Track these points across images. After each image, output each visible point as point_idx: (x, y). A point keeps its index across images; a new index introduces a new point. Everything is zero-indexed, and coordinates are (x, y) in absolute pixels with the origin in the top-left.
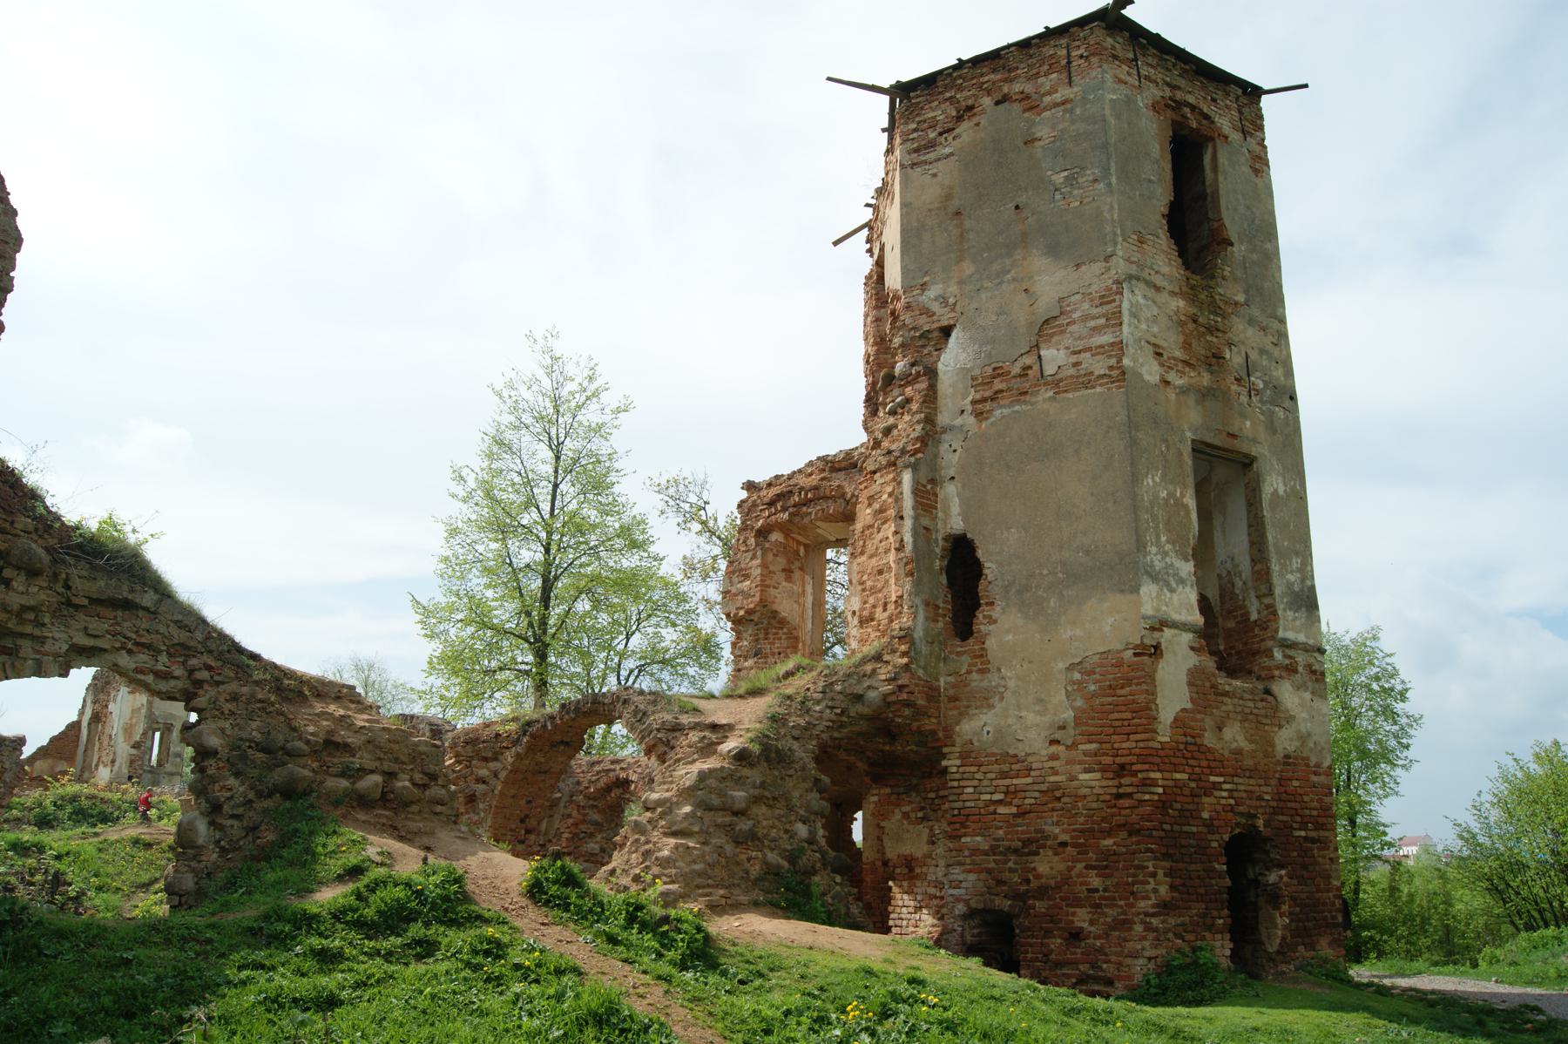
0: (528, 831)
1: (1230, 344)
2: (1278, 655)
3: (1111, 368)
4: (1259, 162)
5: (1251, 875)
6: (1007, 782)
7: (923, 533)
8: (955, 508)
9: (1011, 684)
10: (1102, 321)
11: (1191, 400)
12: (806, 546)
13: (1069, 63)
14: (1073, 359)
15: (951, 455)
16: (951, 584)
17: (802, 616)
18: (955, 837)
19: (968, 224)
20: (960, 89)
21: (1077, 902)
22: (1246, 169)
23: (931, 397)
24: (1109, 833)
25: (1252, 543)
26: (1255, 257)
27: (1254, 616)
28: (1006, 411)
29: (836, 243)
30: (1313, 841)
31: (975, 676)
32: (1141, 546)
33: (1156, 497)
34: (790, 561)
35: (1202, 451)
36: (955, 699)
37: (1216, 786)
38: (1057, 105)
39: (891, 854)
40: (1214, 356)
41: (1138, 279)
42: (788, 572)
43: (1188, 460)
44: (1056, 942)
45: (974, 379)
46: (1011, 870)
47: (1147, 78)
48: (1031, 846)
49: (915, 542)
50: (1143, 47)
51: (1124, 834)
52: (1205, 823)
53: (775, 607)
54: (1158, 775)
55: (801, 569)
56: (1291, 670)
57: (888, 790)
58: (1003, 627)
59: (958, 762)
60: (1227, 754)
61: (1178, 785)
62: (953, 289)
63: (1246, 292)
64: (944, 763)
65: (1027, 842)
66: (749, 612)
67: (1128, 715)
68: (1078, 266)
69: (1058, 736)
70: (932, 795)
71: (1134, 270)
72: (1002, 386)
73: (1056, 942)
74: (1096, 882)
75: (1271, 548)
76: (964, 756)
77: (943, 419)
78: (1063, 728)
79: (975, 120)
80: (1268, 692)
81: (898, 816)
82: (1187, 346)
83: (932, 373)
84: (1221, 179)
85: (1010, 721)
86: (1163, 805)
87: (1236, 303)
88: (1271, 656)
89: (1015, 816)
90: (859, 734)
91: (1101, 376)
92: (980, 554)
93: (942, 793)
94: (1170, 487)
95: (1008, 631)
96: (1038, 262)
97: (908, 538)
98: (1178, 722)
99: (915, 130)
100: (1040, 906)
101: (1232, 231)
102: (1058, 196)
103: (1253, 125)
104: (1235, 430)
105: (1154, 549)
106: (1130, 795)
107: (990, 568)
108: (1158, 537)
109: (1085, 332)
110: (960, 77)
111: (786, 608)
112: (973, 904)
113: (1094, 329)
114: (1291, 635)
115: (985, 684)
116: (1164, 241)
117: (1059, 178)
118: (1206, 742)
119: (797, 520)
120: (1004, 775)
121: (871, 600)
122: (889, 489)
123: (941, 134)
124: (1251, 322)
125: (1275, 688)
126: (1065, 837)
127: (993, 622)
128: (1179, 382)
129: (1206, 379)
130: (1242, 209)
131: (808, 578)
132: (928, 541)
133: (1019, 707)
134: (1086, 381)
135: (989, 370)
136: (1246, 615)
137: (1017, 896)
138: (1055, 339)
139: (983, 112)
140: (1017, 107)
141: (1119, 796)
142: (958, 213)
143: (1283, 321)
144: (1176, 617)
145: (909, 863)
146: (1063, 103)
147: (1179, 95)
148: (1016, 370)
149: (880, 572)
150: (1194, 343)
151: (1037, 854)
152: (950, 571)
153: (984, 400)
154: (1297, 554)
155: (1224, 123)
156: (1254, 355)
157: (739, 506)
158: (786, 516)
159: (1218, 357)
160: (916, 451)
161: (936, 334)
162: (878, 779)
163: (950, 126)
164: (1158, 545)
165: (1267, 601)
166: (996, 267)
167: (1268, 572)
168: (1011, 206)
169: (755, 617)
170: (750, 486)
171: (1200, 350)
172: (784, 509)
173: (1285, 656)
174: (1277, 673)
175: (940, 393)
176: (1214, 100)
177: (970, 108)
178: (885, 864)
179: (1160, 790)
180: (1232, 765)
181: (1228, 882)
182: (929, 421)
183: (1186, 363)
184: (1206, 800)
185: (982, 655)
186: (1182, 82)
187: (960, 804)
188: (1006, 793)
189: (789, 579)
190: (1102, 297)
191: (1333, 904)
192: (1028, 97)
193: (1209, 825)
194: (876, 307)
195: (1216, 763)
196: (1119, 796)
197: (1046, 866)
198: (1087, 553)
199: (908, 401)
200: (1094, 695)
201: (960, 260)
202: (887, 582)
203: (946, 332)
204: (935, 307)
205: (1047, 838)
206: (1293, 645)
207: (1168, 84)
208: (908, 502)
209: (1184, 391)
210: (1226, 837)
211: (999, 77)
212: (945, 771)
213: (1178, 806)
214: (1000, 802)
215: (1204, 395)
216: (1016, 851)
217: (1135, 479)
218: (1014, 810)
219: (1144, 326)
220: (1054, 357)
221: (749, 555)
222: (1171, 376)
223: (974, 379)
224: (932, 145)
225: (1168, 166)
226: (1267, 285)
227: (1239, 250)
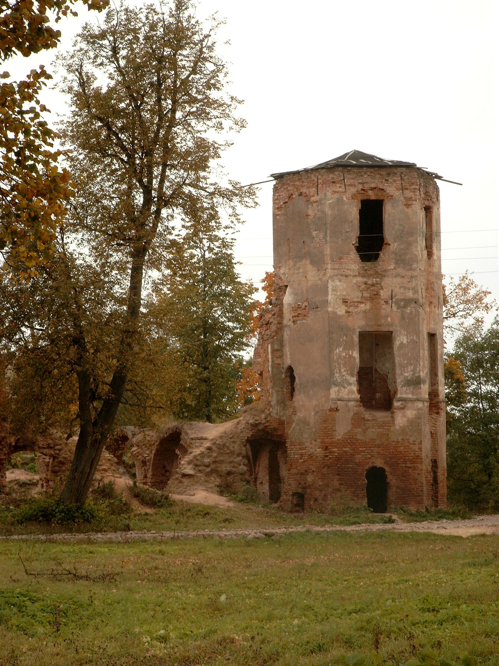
0: (166, 471)
13: (318, 185)
15: (286, 334)
19: (291, 245)
32: (332, 374)
35: (142, 461)
45: (293, 308)
47: (351, 185)
54: (336, 449)
58: (299, 398)
60: (368, 440)
62: (287, 271)
68: (318, 270)
77: (285, 322)
94: (347, 351)
108: (340, 370)
114: (404, 396)
118: (358, 437)
120: (300, 449)
137: (304, 488)
159: (378, 294)
168: (302, 241)
179: (336, 454)
198: (319, 376)
201: (289, 259)
203: (287, 286)
205: (310, 469)
207: (360, 183)
213: (344, 459)
217: (331, 351)
218: (302, 461)
223: (293, 308)
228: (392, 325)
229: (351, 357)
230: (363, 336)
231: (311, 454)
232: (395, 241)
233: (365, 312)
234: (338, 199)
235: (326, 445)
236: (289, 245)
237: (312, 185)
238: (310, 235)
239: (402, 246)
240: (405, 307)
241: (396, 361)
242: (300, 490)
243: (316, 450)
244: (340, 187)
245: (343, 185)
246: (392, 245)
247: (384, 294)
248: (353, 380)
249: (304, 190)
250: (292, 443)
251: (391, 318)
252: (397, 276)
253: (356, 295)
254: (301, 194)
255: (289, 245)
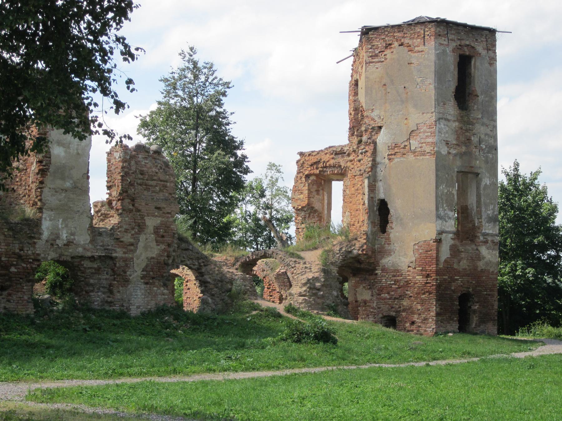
1: (474, 134)
2: (481, 238)
3: (431, 150)
4: (493, 60)
5: (469, 305)
6: (395, 278)
7: (371, 199)
8: (382, 190)
9: (397, 249)
10: (430, 134)
11: (458, 158)
12: (324, 181)
13: (424, 37)
14: (420, 145)
16: (380, 215)
17: (323, 208)
18: (379, 295)
20: (387, 36)
22: (487, 65)
24: (424, 294)
25: (477, 201)
26: (487, 99)
27: (476, 225)
28: (399, 160)
29: (337, 63)
30: (489, 295)
31: (386, 245)
33: (443, 192)
34: (318, 187)
36: (380, 252)
37: (457, 280)
38: (419, 52)
39: (359, 298)
40: (468, 140)
41: (442, 119)
42: (318, 191)
44: (408, 325)
46: (396, 304)
47: (452, 40)
49: (369, 203)
50: (451, 27)
51: (428, 294)
52: (452, 290)
53: (313, 206)
55: (323, 189)
56: (486, 242)
57: (358, 279)
58: (395, 230)
59: (381, 272)
60: (461, 270)
61: (445, 280)
62: (383, 113)
63: (482, 113)
64: (377, 272)
65: (400, 296)
66: (303, 207)
67: (430, 260)
69: (410, 265)
70: (372, 281)
71: (441, 116)
72: (398, 151)
74: (419, 307)
75: (483, 203)
77: (378, 159)
78: (412, 262)
79: (392, 50)
80: (477, 249)
81: (361, 287)
82: (458, 139)
83: (375, 143)
84: (476, 71)
85: (397, 260)
87: (478, 119)
88: (479, 239)
89: (397, 288)
90: (350, 263)
91: (428, 153)
92: (389, 206)
93: (376, 280)
94: (448, 189)
95: (397, 232)
97: (366, 202)
98: (446, 261)
99: (371, 48)
101: (479, 92)
102: (418, 87)
103: (491, 46)
104: (473, 165)
105: (441, 209)
106: (430, 283)
107: (392, 211)
108: (443, 205)
109: (424, 137)
110: (387, 31)
111: (317, 206)
112: (384, 314)
113: (427, 136)
114: (487, 231)
115: (389, 248)
117: (419, 80)
119: (322, 173)
120: (394, 276)
121: (354, 219)
122: (360, 183)
123: (380, 52)
124: (483, 124)
125: (479, 248)
126: (411, 295)
127: (392, 228)
128: (454, 152)
129: (464, 149)
130: (484, 82)
131: (325, 193)
132: (373, 202)
133: (399, 256)
134: (423, 153)
135: (394, 145)
136: (474, 223)
137: (398, 312)
138: (415, 137)
139: (395, 48)
140: (406, 49)
141: (427, 283)
142: (385, 85)
143: (495, 121)
144: (447, 230)
145: (365, 302)
146: (422, 51)
147: (463, 43)
148: (402, 146)
149: (357, 210)
150: (461, 137)
151: (403, 299)
152: (380, 210)
153: (391, 155)
154: (492, 204)
155: (480, 49)
156: (482, 136)
157: (297, 162)
158: (318, 172)
159: (469, 139)
160: (369, 172)
161: (376, 128)
162: (354, 275)
163: (383, 50)
164: (443, 207)
165: (480, 220)
167: (481, 211)
168: (403, 86)
169: (305, 209)
170: (301, 154)
172: (317, 168)
173: (484, 238)
174: (481, 244)
175: (377, 150)
176: (476, 40)
177: (390, 44)
178: (356, 301)
181: (459, 307)
182: (374, 160)
183: (457, 145)
184: (453, 284)
187: (381, 285)
188: (395, 281)
189: (318, 194)
190: (430, 126)
191: (494, 314)
192: (410, 46)
193: (454, 291)
194: (354, 96)
195: (458, 273)
196: (427, 283)
199: (367, 151)
200: (421, 254)
202: (359, 214)
203: (380, 128)
204: (376, 118)
205: (407, 295)
206: (488, 234)
208: (366, 190)
209: (455, 155)
210: (459, 294)
211: (400, 35)
212: (376, 274)
214: (393, 284)
215: (462, 155)
216: (397, 299)
218: (397, 286)
219: (443, 135)
220: (414, 144)
221: (303, 185)
222: (451, 151)
224: (376, 56)
225: (456, 73)
226: (490, 109)
227: (481, 98)
229: (451, 194)
231: (407, 281)
232: (482, 94)
234: (443, 50)
235: (427, 273)
237: (416, 36)
239: (487, 99)
241: (482, 199)
243: (414, 277)
244: (444, 40)
245: (447, 39)
246: (480, 97)
249: (406, 41)
250: (383, 270)
254: (402, 45)
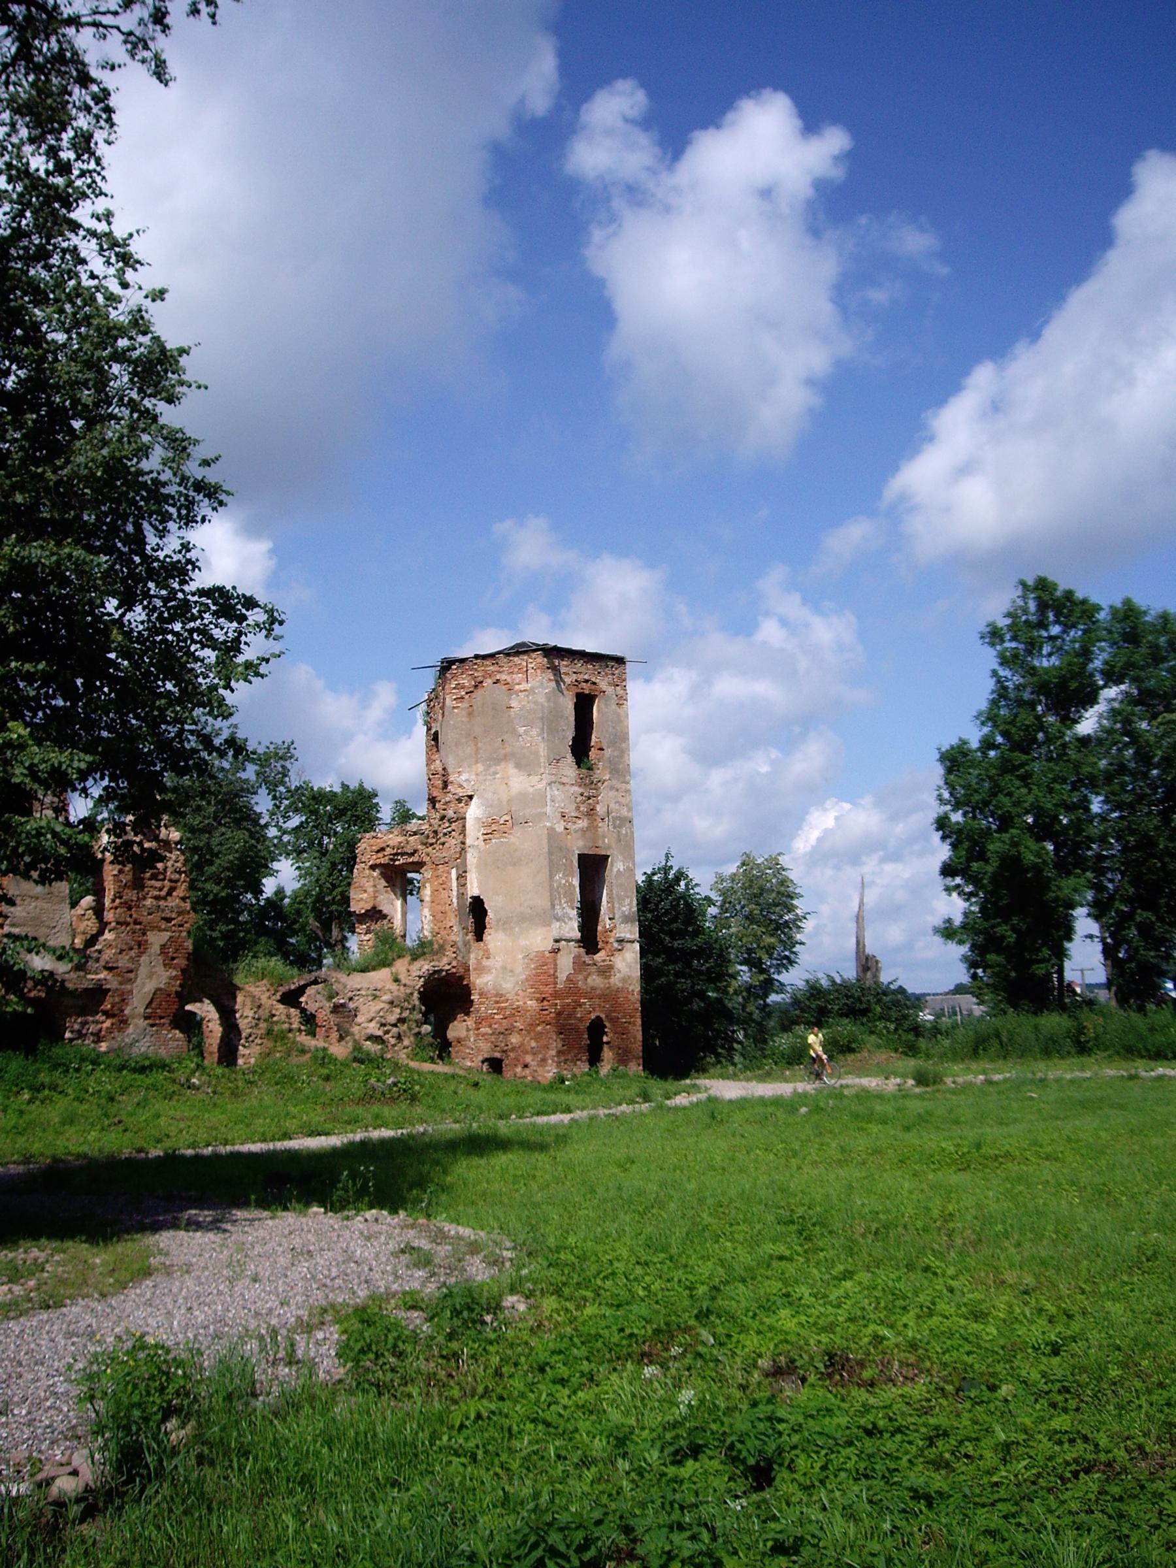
19: (480, 745)
21: (527, 1053)
23: (463, 832)
37: (584, 1004)
43: (576, 864)
44: (519, 1069)
48: (509, 1030)
58: (493, 937)
62: (473, 777)
73: (519, 1069)
76: (481, 995)
77: (468, 842)
86: (559, 1014)
96: (511, 770)
100: (512, 1055)
116: (570, 759)
120: (497, 1002)
156: (612, 805)
166: (492, 769)
171: (583, 808)
180: (590, 994)
185: (487, 950)
186: (583, 669)
193: (581, 1020)
197: (515, 1039)
201: (477, 762)
203: (471, 797)
217: (551, 877)
228: (609, 848)
229: (571, 885)
230: (582, 858)
233: (582, 830)
236: (476, 745)
238: (514, 732)
240: (620, 826)
242: (497, 1055)
247: (600, 809)
248: (574, 913)
249: (503, 677)
251: (607, 842)
252: (612, 788)
253: (571, 810)
255: (476, 745)
